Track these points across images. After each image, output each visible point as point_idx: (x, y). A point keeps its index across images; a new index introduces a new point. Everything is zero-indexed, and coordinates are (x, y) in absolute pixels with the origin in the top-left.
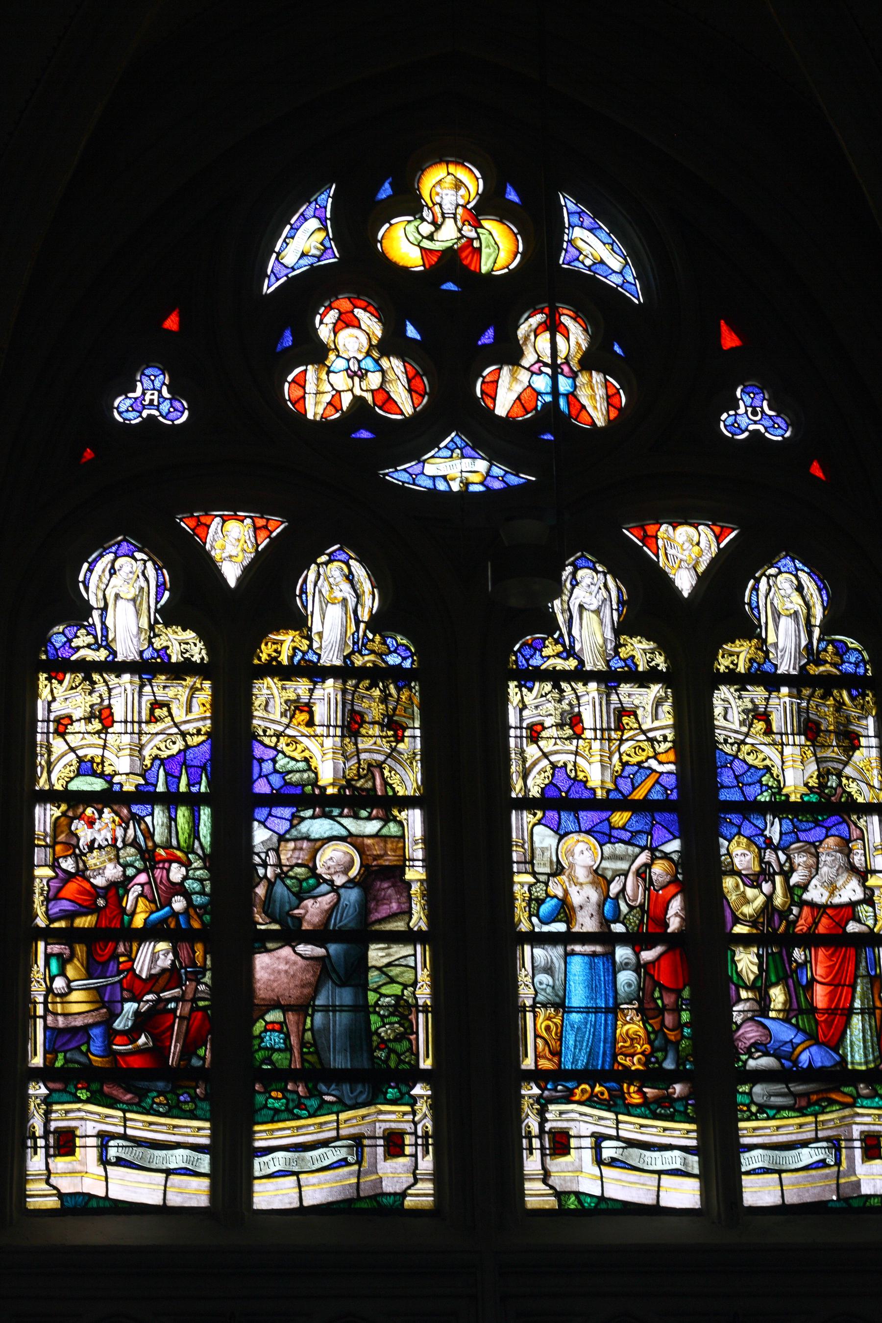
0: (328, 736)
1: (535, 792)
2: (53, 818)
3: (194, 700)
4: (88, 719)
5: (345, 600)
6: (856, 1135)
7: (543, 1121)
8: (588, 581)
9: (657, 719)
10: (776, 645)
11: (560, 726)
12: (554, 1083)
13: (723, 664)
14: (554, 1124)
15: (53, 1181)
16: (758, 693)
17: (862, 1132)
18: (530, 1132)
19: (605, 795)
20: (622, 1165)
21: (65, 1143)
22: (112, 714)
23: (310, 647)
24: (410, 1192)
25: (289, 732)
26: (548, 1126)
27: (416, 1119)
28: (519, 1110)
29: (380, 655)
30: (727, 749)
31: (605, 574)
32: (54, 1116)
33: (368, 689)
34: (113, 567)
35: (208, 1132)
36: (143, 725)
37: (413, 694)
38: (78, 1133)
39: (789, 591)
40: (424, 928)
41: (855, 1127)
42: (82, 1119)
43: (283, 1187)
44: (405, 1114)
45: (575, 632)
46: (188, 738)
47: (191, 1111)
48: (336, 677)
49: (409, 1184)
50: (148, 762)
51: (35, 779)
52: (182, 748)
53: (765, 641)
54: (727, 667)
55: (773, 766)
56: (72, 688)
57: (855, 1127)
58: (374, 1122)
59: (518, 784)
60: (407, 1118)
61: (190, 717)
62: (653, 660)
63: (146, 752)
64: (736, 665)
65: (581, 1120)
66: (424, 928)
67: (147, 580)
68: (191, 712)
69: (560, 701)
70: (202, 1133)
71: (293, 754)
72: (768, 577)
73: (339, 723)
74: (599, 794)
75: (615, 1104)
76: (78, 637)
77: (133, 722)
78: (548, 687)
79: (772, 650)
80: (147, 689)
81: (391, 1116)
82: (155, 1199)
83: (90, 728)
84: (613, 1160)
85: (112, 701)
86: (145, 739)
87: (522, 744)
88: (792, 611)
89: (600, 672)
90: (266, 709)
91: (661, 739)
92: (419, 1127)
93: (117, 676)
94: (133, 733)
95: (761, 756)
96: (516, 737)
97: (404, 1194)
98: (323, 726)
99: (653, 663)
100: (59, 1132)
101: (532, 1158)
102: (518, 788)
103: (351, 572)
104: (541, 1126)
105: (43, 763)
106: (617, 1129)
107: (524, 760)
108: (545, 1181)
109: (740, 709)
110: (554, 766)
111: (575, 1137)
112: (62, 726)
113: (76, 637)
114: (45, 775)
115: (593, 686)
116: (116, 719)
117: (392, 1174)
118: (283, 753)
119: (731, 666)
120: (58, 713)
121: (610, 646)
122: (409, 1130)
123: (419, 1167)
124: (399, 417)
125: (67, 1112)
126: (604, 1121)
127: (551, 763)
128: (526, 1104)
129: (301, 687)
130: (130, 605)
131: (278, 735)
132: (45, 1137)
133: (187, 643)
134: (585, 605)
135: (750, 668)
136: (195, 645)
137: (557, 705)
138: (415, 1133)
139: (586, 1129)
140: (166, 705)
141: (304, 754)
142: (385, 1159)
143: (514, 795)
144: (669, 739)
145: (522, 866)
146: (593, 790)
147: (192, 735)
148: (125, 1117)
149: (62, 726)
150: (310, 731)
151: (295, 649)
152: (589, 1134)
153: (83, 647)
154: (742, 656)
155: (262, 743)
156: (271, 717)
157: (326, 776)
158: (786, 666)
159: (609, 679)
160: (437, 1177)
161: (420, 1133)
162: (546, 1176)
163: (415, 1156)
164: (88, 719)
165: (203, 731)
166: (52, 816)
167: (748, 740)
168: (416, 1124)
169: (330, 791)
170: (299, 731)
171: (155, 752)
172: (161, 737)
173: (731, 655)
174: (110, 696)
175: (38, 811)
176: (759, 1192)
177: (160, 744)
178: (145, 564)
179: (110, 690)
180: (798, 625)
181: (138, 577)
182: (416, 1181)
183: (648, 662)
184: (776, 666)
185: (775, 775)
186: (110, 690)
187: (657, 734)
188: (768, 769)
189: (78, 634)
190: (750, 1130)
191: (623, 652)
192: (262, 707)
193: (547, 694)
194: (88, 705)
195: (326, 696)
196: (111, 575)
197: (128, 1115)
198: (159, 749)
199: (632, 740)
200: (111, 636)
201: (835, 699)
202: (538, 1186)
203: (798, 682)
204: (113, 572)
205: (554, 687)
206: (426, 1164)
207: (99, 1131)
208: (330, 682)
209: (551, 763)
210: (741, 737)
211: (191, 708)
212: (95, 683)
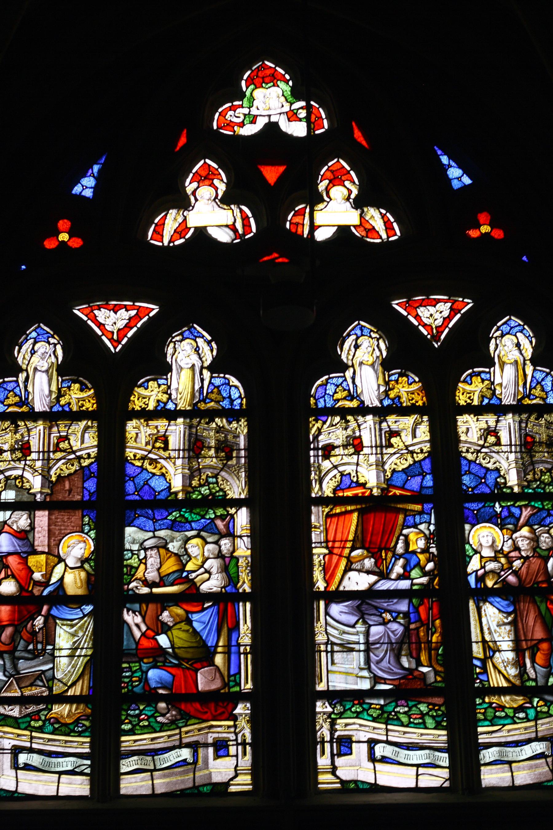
0: (511, 452)
1: (328, 492)
2: (325, 513)
3: (417, 430)
4: (13, 450)
5: (516, 362)
7: (333, 730)
8: (42, 350)
9: (415, 437)
10: (501, 385)
14: (343, 733)
15: (338, 773)
16: (491, 419)
19: (520, 490)
20: (181, 763)
22: (361, 442)
23: (170, 398)
24: (231, 782)
25: (151, 456)
26: (337, 734)
27: (237, 730)
28: (314, 722)
29: (218, 402)
30: (470, 456)
31: (378, 340)
33: (207, 423)
35: (445, 738)
36: (384, 449)
37: (241, 428)
38: (354, 739)
39: (189, 351)
43: (74, 782)
44: (229, 727)
46: (415, 455)
48: (44, 420)
49: (231, 777)
50: (389, 474)
51: (309, 488)
52: (412, 463)
54: (140, 407)
55: (167, 473)
56: (333, 426)
58: (207, 733)
59: (316, 488)
60: (232, 730)
61: (415, 441)
62: (413, 399)
63: (387, 467)
64: (472, 400)
65: (361, 729)
68: (415, 437)
69: (346, 429)
71: (154, 471)
72: (496, 338)
75: (386, 718)
76: (9, 398)
78: (337, 419)
79: (498, 388)
80: (55, 429)
81: (221, 729)
82: (52, 792)
83: (346, 452)
87: (318, 460)
88: (512, 361)
92: (240, 736)
93: (363, 416)
97: (227, 784)
98: (175, 450)
102: (316, 490)
103: (197, 346)
104: (332, 735)
105: (316, 477)
106: (387, 735)
107: (320, 472)
109: (147, 434)
110: (342, 474)
111: (356, 742)
112: (328, 451)
114: (318, 486)
115: (370, 418)
116: (32, 450)
117: (220, 769)
118: (146, 469)
119: (469, 401)
121: (54, 396)
122: (232, 738)
123: (239, 765)
124: (379, 241)
125: (346, 725)
126: (378, 731)
127: (339, 472)
129: (162, 424)
130: (370, 370)
131: (143, 458)
132: (331, 742)
134: (39, 368)
135: (156, 407)
136: (418, 394)
137: (344, 432)
139: (364, 736)
141: (495, 465)
142: (215, 759)
143: (313, 495)
144: (92, 456)
146: (511, 488)
147: (417, 453)
148: (386, 728)
150: (166, 454)
153: (341, 399)
154: (152, 399)
155: (134, 465)
157: (513, 479)
158: (508, 400)
159: (381, 413)
160: (255, 771)
162: (334, 770)
164: (345, 446)
168: (236, 734)
169: (180, 496)
171: (393, 466)
172: (63, 461)
173: (144, 398)
174: (29, 434)
176: (132, 785)
177: (396, 462)
178: (55, 346)
179: (359, 426)
182: (236, 776)
184: (176, 405)
185: (168, 480)
186: (359, 426)
187: (416, 448)
189: (337, 390)
191: (392, 394)
192: (133, 439)
193: (336, 425)
194: (344, 437)
195: (507, 426)
196: (32, 354)
198: (62, 470)
201: (217, 424)
202: (329, 777)
203: (517, 409)
205: (341, 419)
206: (246, 762)
207: (369, 739)
208: (180, 420)
210: (479, 448)
212: (349, 421)
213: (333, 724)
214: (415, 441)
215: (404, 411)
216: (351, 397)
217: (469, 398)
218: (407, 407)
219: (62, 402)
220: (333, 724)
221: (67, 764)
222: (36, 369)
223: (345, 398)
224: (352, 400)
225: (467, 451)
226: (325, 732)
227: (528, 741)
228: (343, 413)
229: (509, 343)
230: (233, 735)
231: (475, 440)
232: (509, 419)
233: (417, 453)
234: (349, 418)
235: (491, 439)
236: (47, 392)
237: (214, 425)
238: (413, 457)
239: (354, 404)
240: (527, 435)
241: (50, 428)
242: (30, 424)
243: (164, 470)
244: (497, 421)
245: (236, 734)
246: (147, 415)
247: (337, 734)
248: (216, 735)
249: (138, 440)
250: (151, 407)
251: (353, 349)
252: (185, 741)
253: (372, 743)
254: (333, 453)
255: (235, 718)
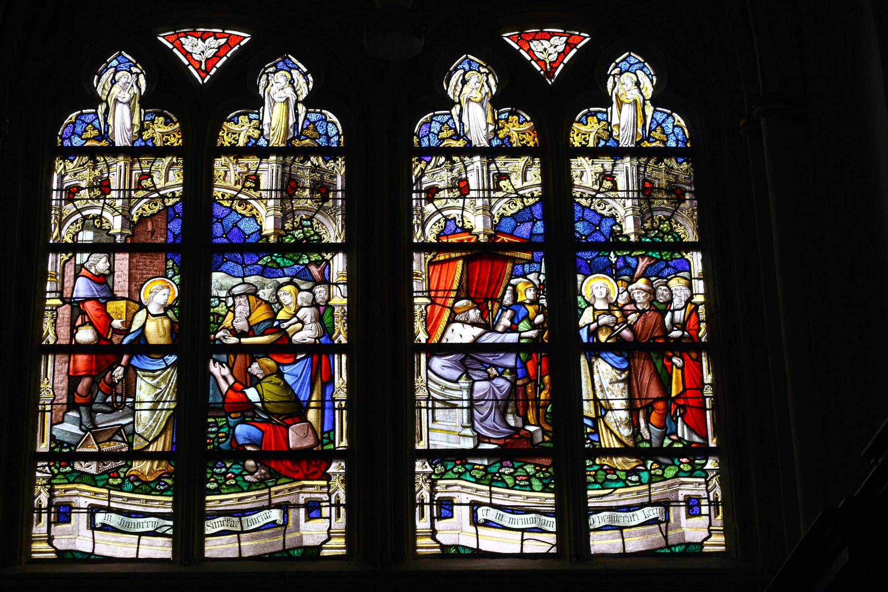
0: (628, 198)
1: (431, 239)
4: (91, 188)
5: (635, 101)
6: (681, 498)
7: (433, 492)
8: (123, 80)
10: (618, 126)
11: (450, 189)
12: (591, 459)
13: (226, 140)
14: (443, 495)
17: (685, 496)
18: (40, 505)
19: (637, 239)
21: (63, 513)
22: (468, 185)
23: (262, 134)
25: (240, 196)
27: (331, 491)
29: (313, 139)
30: (583, 202)
32: (56, 493)
34: (114, 78)
35: (553, 501)
36: (133, 192)
37: (339, 167)
38: (455, 501)
40: (344, 341)
41: (301, 495)
42: (77, 495)
44: (322, 487)
45: (110, 121)
47: (216, 489)
50: (496, 219)
51: (49, 233)
53: (610, 124)
54: (230, 143)
57: (680, 492)
58: (299, 493)
60: (325, 490)
61: (525, 184)
62: (524, 139)
63: (494, 212)
65: (462, 491)
66: (344, 341)
67: (489, 87)
69: (451, 170)
70: (548, 501)
71: (244, 212)
72: (614, 76)
73: (279, 187)
74: (633, 238)
75: (490, 479)
77: (124, 190)
78: (85, 159)
79: (615, 129)
80: (137, 166)
81: (313, 489)
83: (451, 195)
84: (103, 525)
85: (469, 175)
86: (133, 201)
88: (631, 100)
89: (484, 147)
90: (224, 179)
91: (170, 196)
94: (484, 198)
95: (608, 207)
96: (416, 199)
99: (524, 142)
100: (59, 505)
101: (40, 525)
102: (418, 235)
103: (292, 79)
106: (491, 498)
108: (433, 537)
110: (446, 219)
112: (432, 193)
113: (86, 131)
115: (477, 158)
118: (236, 211)
120: (68, 184)
125: (448, 486)
126: (481, 493)
127: (444, 216)
128: (419, 480)
130: (126, 108)
131: (232, 198)
133: (524, 134)
135: (247, 144)
136: (530, 135)
137: (450, 174)
138: (708, 498)
140: (506, 177)
143: (415, 241)
145: (53, 295)
146: (627, 236)
147: (528, 198)
148: (490, 490)
149: (71, 194)
151: (249, 137)
152: (468, 502)
153: (447, 138)
154: (242, 134)
155: (222, 205)
156: (228, 184)
157: (629, 227)
158: (626, 142)
161: (712, 499)
162: (433, 534)
163: (330, 518)
165: (178, 194)
166: (61, 260)
167: (598, 196)
168: (330, 495)
169: (272, 239)
170: (248, 195)
171: (502, 211)
173: (234, 134)
175: (51, 257)
176: (217, 548)
179: (465, 167)
180: (288, 109)
181: (483, 85)
183: (164, 142)
186: (465, 167)
187: (526, 192)
188: (613, 217)
190: (595, 496)
193: (84, 164)
195: (625, 171)
196: (113, 85)
197: (112, 492)
198: (144, 209)
199: (147, 198)
200: (466, 130)
201: (312, 163)
203: (636, 152)
204: (464, 82)
208: (273, 158)
209: (444, 216)
210: (594, 193)
211: (525, 178)
212: (454, 162)
213: (433, 485)
214: (525, 184)
215: (514, 153)
216: (457, 136)
217: (584, 139)
218: (517, 147)
219: (501, 136)
220: (433, 485)
221: (148, 524)
222: (116, 100)
223: (450, 138)
224: (458, 140)
225: (581, 197)
226: (424, 493)
227: (641, 506)
228: (449, 153)
229: (628, 82)
230: (326, 495)
231: (590, 185)
232: (626, 163)
233: (528, 198)
234: (455, 158)
235: (607, 184)
236: (128, 126)
237: (309, 164)
238: (523, 202)
239: (461, 143)
240: (645, 180)
241: (132, 164)
242: (110, 160)
243: (254, 212)
244: (614, 165)
245: (330, 495)
246: (236, 152)
247: (437, 496)
248: (308, 496)
249: (227, 179)
250: (241, 143)
251: (460, 85)
252: (274, 501)
253: (474, 506)
254: (437, 196)
255: (328, 478)
